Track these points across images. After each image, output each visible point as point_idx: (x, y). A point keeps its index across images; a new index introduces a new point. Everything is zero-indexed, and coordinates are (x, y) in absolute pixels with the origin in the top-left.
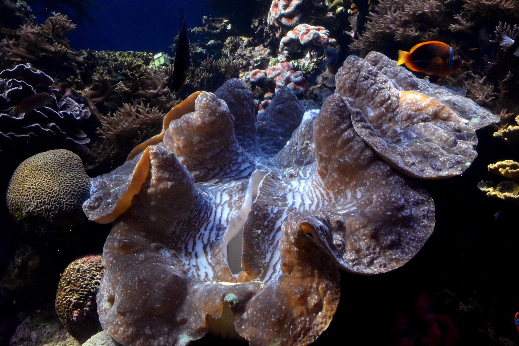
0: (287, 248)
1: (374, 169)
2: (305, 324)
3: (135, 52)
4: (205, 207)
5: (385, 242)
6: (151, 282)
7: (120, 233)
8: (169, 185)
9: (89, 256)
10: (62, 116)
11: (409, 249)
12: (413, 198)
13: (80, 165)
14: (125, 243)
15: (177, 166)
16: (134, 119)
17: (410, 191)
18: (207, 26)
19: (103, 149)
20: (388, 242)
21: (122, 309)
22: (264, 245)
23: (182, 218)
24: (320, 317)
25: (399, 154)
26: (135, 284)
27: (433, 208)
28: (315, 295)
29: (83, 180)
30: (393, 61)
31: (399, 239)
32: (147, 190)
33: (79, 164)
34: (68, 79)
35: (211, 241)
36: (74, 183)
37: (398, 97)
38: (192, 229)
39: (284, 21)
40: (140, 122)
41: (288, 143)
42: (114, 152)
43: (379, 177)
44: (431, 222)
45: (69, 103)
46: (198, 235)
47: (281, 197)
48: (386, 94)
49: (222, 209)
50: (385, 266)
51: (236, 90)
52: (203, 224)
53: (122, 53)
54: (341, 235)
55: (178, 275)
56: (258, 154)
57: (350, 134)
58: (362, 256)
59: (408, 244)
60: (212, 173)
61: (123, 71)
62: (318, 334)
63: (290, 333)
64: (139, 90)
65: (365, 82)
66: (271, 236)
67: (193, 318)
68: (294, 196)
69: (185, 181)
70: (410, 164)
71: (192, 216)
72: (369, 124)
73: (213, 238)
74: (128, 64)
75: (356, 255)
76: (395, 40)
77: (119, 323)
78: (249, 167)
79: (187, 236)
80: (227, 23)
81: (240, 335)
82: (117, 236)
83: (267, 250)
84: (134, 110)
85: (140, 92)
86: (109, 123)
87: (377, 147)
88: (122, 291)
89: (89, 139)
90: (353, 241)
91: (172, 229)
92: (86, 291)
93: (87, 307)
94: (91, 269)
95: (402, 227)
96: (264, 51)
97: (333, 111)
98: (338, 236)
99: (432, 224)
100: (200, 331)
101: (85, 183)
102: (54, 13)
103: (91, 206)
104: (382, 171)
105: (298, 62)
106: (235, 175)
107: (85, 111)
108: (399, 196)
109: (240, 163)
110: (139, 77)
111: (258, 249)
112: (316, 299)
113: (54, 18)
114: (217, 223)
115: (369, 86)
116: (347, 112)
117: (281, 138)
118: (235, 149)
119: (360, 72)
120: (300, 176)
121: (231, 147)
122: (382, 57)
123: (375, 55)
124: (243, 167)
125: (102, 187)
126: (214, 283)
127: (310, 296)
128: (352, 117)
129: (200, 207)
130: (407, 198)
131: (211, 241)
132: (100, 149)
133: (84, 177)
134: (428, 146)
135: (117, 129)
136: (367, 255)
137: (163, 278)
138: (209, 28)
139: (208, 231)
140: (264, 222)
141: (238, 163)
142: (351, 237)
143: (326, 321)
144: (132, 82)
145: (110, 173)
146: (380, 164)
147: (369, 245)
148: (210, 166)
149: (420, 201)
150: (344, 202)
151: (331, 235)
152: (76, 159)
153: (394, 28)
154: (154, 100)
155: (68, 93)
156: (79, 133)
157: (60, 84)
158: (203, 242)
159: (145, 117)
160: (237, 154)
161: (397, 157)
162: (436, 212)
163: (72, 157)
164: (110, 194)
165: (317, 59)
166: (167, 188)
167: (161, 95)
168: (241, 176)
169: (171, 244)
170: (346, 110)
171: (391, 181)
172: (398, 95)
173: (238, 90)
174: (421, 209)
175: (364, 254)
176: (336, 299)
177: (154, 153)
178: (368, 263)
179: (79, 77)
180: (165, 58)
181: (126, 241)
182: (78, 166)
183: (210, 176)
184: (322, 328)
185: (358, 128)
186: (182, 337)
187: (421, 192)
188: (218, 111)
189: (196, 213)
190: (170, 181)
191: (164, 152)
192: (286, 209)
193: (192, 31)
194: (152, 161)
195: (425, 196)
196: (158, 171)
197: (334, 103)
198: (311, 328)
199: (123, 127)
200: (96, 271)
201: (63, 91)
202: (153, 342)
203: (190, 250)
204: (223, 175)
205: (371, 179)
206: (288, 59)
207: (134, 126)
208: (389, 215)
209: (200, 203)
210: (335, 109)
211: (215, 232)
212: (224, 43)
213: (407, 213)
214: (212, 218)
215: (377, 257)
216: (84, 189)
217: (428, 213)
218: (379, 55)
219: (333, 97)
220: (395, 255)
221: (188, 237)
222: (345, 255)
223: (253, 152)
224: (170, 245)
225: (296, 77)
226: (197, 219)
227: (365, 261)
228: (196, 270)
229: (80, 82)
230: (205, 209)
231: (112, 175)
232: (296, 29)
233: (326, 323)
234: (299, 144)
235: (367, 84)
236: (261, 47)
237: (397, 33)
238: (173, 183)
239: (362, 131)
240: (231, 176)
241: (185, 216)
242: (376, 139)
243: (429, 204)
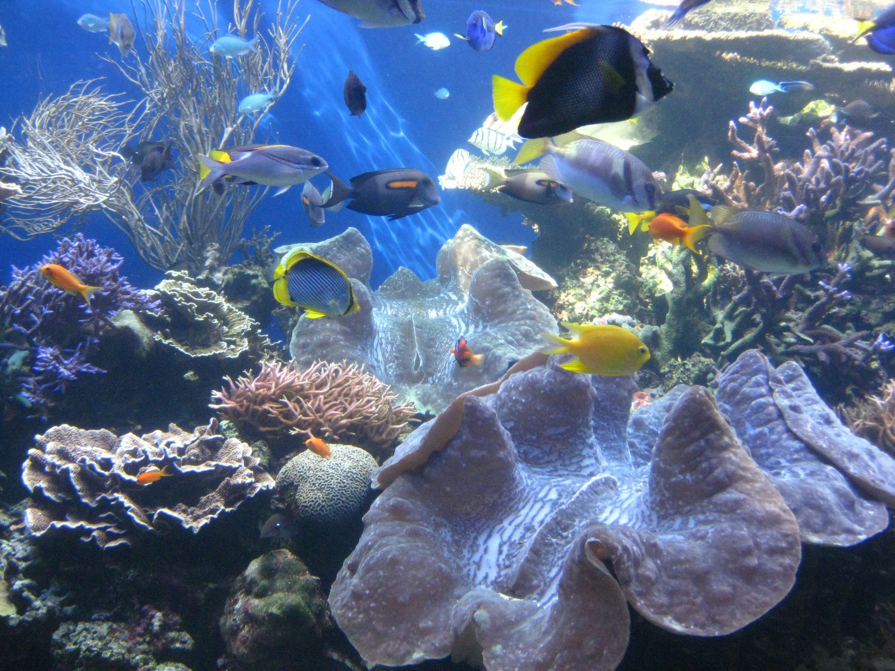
35: (513, 539)
78: (592, 465)
124: (587, 462)
131: (513, 539)
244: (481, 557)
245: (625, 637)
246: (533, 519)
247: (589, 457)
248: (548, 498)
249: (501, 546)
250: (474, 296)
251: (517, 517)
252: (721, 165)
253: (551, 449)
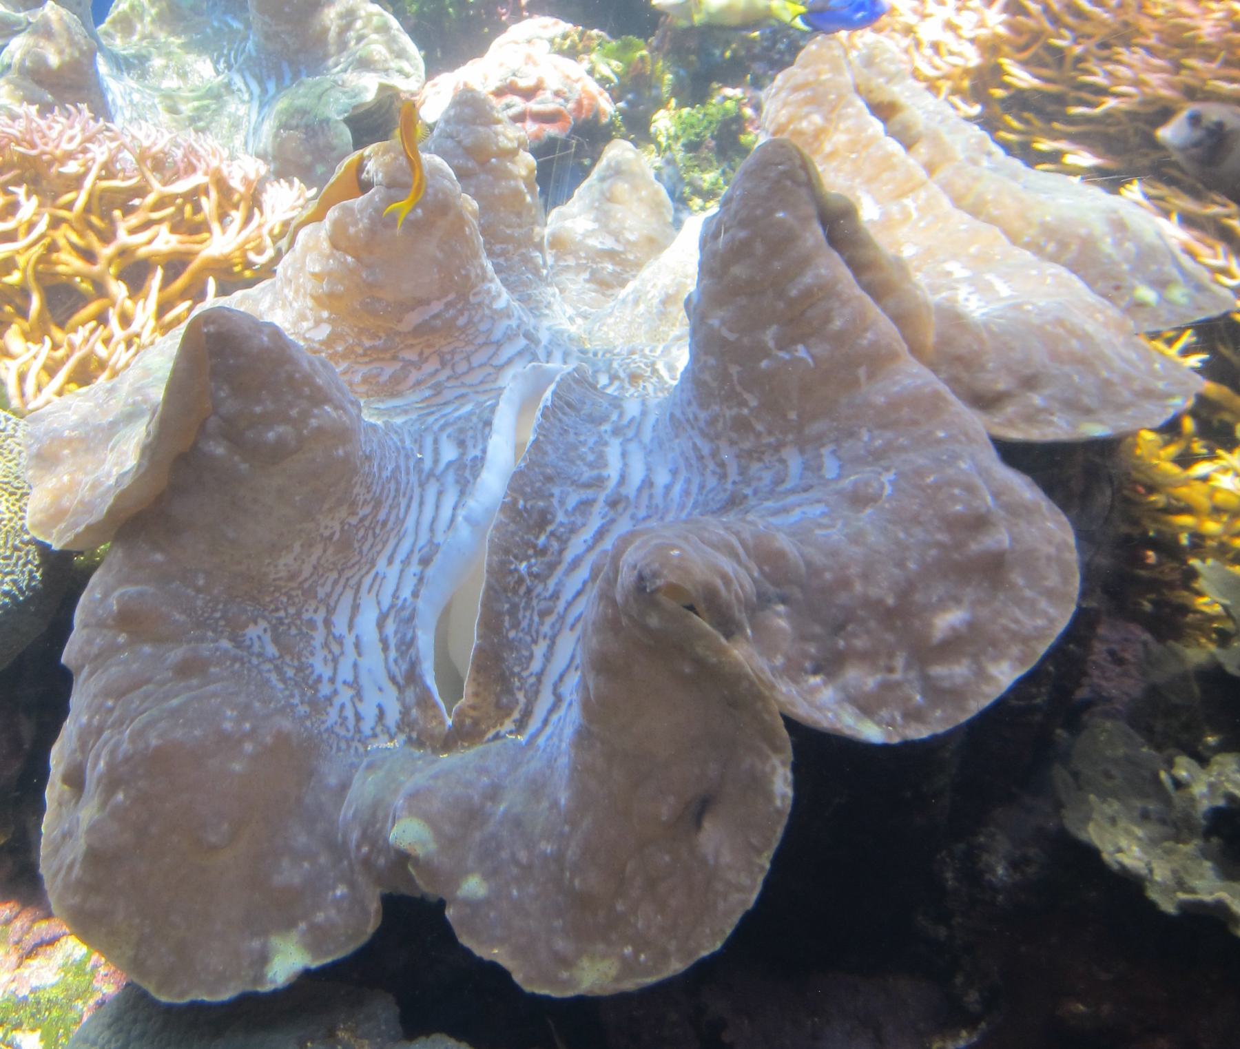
4: (393, 486)
22: (528, 614)
23: (322, 530)
38: (353, 561)
46: (367, 581)
52: (385, 543)
66: (551, 584)
68: (624, 455)
79: (336, 582)
83: (537, 632)
106: (480, 378)
120: (660, 378)
121: (475, 295)
139: (397, 565)
140: (537, 538)
148: (411, 355)
158: (379, 603)
169: (286, 610)
189: (367, 510)
192: (602, 498)
203: (340, 626)
221: (339, 588)
226: (367, 529)
228: (352, 699)
230: (392, 494)
244: (355, 666)
245: (438, 79)
246: (432, 529)
248: (442, 466)
249: (381, 624)
253: (421, 354)
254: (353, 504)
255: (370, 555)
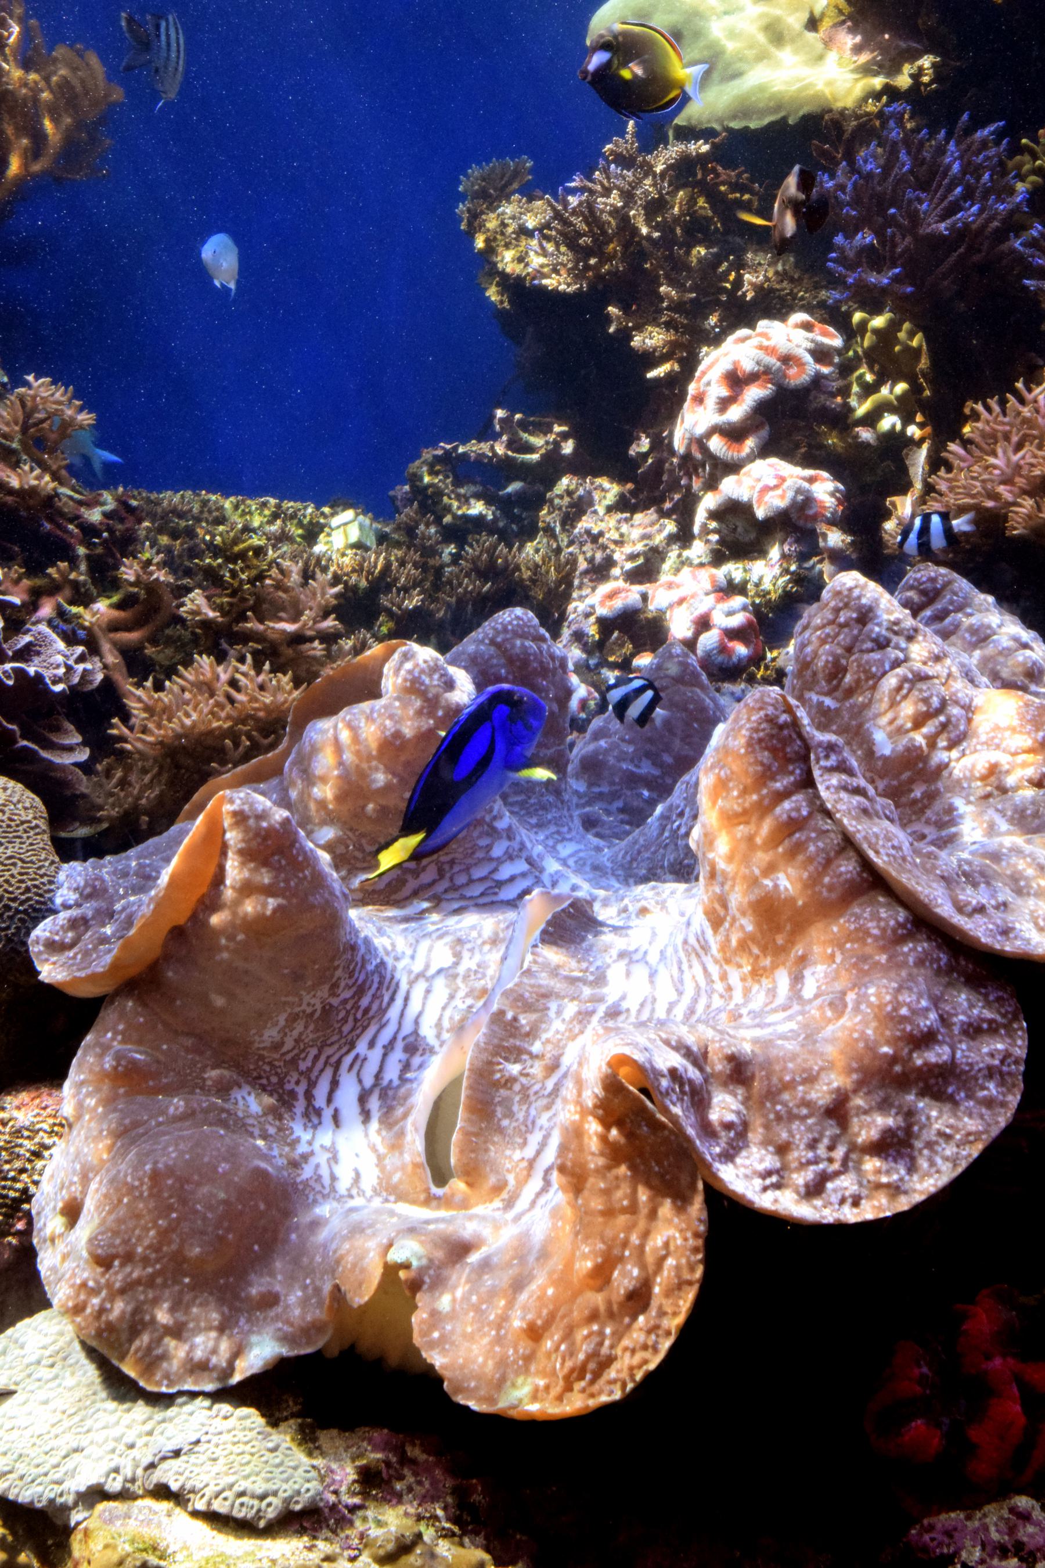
0: (573, 1122)
1: (858, 917)
2: (601, 1344)
3: (282, 501)
4: (376, 979)
5: (863, 1133)
6: (188, 1182)
7: (123, 1033)
8: (270, 907)
9: (38, 1089)
10: (9, 677)
11: (932, 1164)
12: (964, 1013)
13: (37, 826)
14: (134, 1062)
15: (298, 854)
16: (218, 704)
17: (959, 992)
18: (505, 438)
19: (123, 783)
20: (874, 1134)
21: (102, 1247)
24: (641, 1329)
25: (943, 877)
26: (142, 1184)
27: (1020, 1048)
28: (634, 1266)
29: (39, 868)
30: (982, 596)
31: (908, 1131)
32: (210, 916)
33: (35, 822)
34: (50, 570)
35: (385, 1082)
36: (12, 876)
37: (969, 708)
39: (716, 444)
40: (235, 714)
41: (659, 809)
42: (153, 794)
43: (869, 940)
44: (1009, 1091)
45: (42, 639)
46: (348, 1060)
47: (592, 973)
48: (931, 696)
49: (428, 991)
50: (856, 1202)
51: (518, 642)
52: (365, 1028)
53: (243, 501)
54: (740, 1097)
55: (270, 1169)
56: (568, 836)
57: (798, 810)
58: (794, 1165)
59: (930, 1145)
60: (412, 884)
61: (208, 561)
62: (632, 1376)
63: (558, 1366)
64: (246, 619)
65: (876, 656)
67: (299, 1293)
69: (317, 899)
70: (969, 909)
71: (335, 1001)
72: (862, 782)
73: (392, 1073)
74: (223, 542)
75: (776, 1158)
76: (1008, 533)
77: (91, 1284)
78: (524, 875)
79: (316, 1058)
80: (565, 436)
81: (424, 1354)
82: (113, 1039)
83: (533, 1123)
84: (224, 677)
85: (249, 625)
86: (147, 709)
87: (877, 852)
88: (106, 1196)
89: (88, 751)
90: (772, 1116)
91: (271, 1034)
92: (16, 1190)
93: (13, 1235)
94: (38, 1126)
95: (922, 1094)
96: (657, 527)
97: (755, 736)
98: (729, 1098)
99: (1010, 1098)
100: (313, 1332)
101: (45, 880)
102: (30, 378)
103: (54, 942)
104: (882, 924)
105: (745, 570)
106: (477, 893)
107: (85, 670)
108: (924, 1003)
109: (498, 859)
110: (251, 581)
111: (505, 1116)
112: (632, 1278)
113: (31, 392)
114: (407, 1028)
115: (887, 667)
116: (799, 742)
117: (646, 793)
118: (488, 818)
119: (864, 624)
122: (949, 583)
123: (933, 574)
124: (506, 871)
125: (92, 892)
126: (377, 1202)
127: (619, 1267)
128: (812, 756)
129: (362, 977)
130: (948, 1013)
131: (385, 1082)
132: (114, 781)
133: (46, 859)
134: (1034, 859)
135: (166, 728)
136: (809, 1163)
137: (225, 1174)
138: (510, 445)
141: (491, 859)
142: (768, 1105)
143: (656, 1343)
144: (227, 595)
145: (124, 855)
146: (879, 903)
147: (816, 1135)
149: (985, 1026)
150: (767, 1005)
151: (709, 1093)
152: (28, 805)
153: (1008, 497)
154: (289, 652)
155: (47, 610)
156: (58, 729)
157: (26, 583)
158: (360, 1081)
159: (250, 701)
160: (493, 833)
161: (935, 885)
162: (1028, 1061)
163: (19, 801)
164: (111, 914)
165: (800, 567)
166: (264, 914)
167: (311, 640)
168: (495, 898)
169: (268, 1079)
170: (794, 736)
171: (906, 955)
172: (971, 700)
173: (523, 645)
174: (985, 1050)
175: (799, 1159)
176: (690, 1283)
177: (235, 814)
178: (807, 1185)
179: (83, 567)
180: (361, 527)
181: (138, 1056)
182: (32, 828)
183: (407, 891)
184: (646, 1362)
185: (828, 788)
186: (258, 1343)
187: (991, 998)
188: (443, 703)
190: (273, 895)
191: (264, 811)
192: (602, 1009)
193: (461, 450)
194: (228, 835)
195: (1003, 1011)
196: (243, 864)
197: (762, 713)
198: (616, 1358)
199: (183, 725)
200: (51, 1133)
201: (32, 606)
202: (176, 1348)
203: (320, 1101)
204: (446, 891)
205: (848, 945)
206: (718, 558)
207: (215, 724)
208: (886, 1055)
209: (363, 966)
210: (763, 730)
211: (398, 1055)
212: (548, 495)
213: (939, 1055)
214: (393, 1013)
215: (837, 1174)
216: (41, 895)
217: (1002, 1062)
218: (941, 575)
219: (762, 697)
220: (888, 1173)
222: (744, 1153)
223: (553, 828)
224: (264, 1081)
225: (730, 613)
226: (348, 1012)
227: (801, 1179)
228: (328, 1160)
229: (85, 584)
230: (375, 985)
231: (128, 858)
232: (748, 474)
233: (655, 1350)
234: (686, 815)
235: (881, 662)
236: (651, 514)
237: (1017, 513)
238: (280, 901)
239: (841, 799)
240: (469, 894)
241: (312, 1001)
242: (881, 827)
243: (1010, 1037)
247: (511, 858)
250: (296, 708)
251: (382, 1027)
252: (651, 375)
254: (335, 986)
255: (350, 1037)
